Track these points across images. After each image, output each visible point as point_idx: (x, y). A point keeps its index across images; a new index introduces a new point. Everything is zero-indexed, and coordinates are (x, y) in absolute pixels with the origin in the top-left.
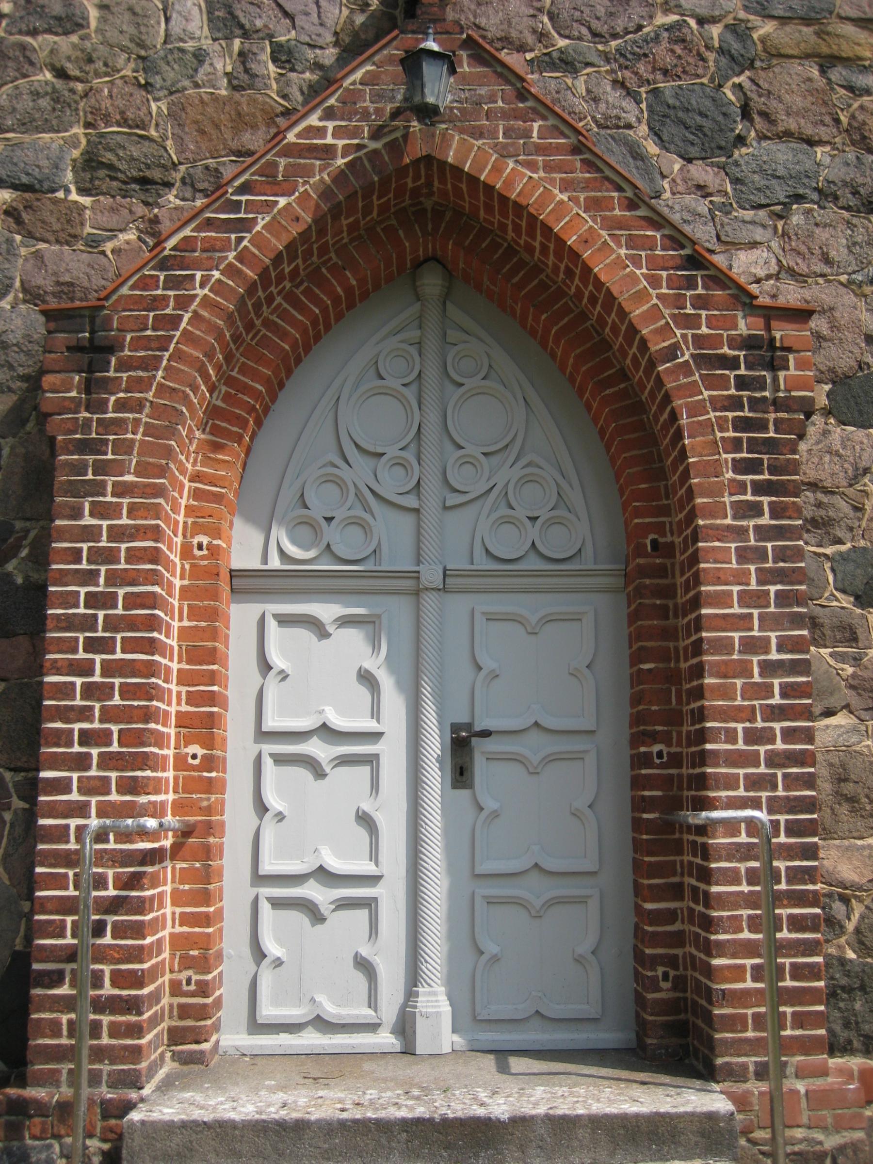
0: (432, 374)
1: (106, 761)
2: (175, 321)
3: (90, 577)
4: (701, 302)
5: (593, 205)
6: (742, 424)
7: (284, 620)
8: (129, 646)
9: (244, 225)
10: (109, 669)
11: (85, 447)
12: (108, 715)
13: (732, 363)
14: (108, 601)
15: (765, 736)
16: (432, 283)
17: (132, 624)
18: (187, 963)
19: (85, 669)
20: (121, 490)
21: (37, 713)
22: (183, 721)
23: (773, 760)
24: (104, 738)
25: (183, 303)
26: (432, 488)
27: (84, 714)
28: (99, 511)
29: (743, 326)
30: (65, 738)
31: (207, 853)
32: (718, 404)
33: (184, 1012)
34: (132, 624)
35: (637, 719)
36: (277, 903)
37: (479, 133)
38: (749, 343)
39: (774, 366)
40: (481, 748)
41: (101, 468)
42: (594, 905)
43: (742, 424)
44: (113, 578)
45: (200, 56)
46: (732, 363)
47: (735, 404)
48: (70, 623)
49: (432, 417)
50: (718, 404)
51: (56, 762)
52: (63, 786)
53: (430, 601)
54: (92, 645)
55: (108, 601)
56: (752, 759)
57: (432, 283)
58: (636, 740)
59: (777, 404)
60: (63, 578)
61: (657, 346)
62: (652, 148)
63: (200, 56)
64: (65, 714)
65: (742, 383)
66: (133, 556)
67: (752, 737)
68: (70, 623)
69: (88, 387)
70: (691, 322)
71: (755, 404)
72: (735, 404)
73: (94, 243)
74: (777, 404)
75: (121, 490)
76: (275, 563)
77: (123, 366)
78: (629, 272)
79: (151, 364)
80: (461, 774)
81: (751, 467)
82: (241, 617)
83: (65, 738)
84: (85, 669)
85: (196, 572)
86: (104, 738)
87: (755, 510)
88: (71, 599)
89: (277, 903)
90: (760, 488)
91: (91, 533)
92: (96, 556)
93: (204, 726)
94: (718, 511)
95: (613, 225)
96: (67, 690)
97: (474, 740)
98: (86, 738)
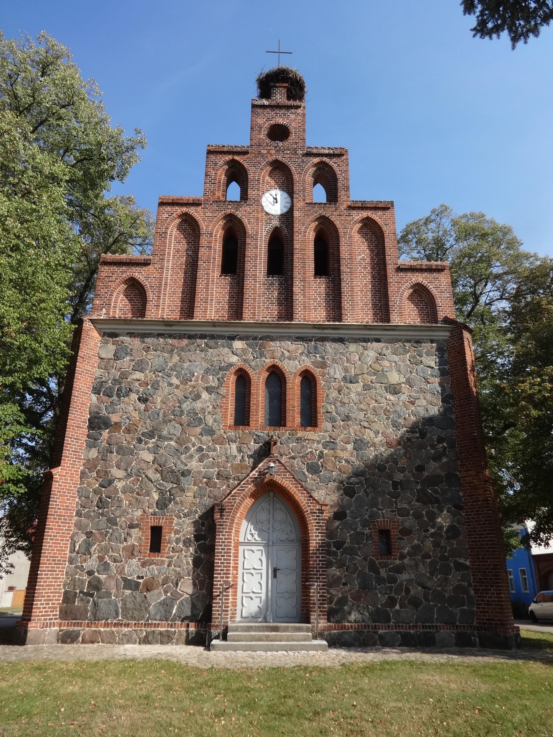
0: (271, 509)
1: (224, 574)
2: (233, 506)
3: (221, 545)
4: (311, 503)
5: (296, 487)
6: (317, 523)
7: (248, 550)
8: (227, 556)
9: (244, 490)
10: (224, 560)
11: (221, 525)
12: (224, 567)
13: (316, 513)
14: (224, 549)
15: (319, 571)
16: (271, 494)
17: (228, 553)
18: (233, 606)
19: (221, 560)
20: (226, 532)
21: (213, 566)
22: (233, 567)
23: (320, 575)
24: (223, 570)
25: (235, 503)
26: (271, 528)
27: (220, 566)
28: (223, 535)
29: (318, 507)
30: (218, 570)
31: (236, 588)
32: (314, 519)
33: (233, 614)
34: (228, 553)
35: (302, 568)
36: (246, 597)
37: (279, 475)
38: (319, 510)
39: (322, 513)
40: (278, 572)
41: (223, 529)
42: (295, 598)
43: (317, 523)
44: (225, 546)
45: (236, 456)
46: (316, 513)
47: (316, 519)
48: (218, 553)
49: (271, 516)
50: (314, 519)
51: (216, 574)
52: (217, 577)
53: (270, 547)
54: (222, 556)
55: (224, 549)
56: (317, 575)
57: (271, 494)
58: (303, 571)
59: (322, 520)
60: (217, 545)
61: (305, 510)
62: (307, 473)
63: (236, 456)
64: (217, 566)
65: (317, 516)
66: (228, 542)
67: (317, 571)
68: (218, 553)
69: (221, 516)
70: (310, 506)
71: (319, 520)
72: (316, 519)
73: (219, 488)
74: (322, 520)
75: (226, 532)
76: (246, 541)
77: (226, 512)
78: (301, 498)
79: (230, 512)
80: (275, 576)
81: (318, 529)
82: (241, 548)
83: (218, 570)
84: (221, 560)
85: (235, 543)
86: (223, 570)
87: (318, 536)
88: (218, 549)
89: (246, 597)
90: (319, 533)
91: (221, 539)
92: (223, 542)
93: (236, 568)
94: (313, 536)
95: (298, 490)
96: (218, 563)
97: (239, 200)
98: (221, 570)
